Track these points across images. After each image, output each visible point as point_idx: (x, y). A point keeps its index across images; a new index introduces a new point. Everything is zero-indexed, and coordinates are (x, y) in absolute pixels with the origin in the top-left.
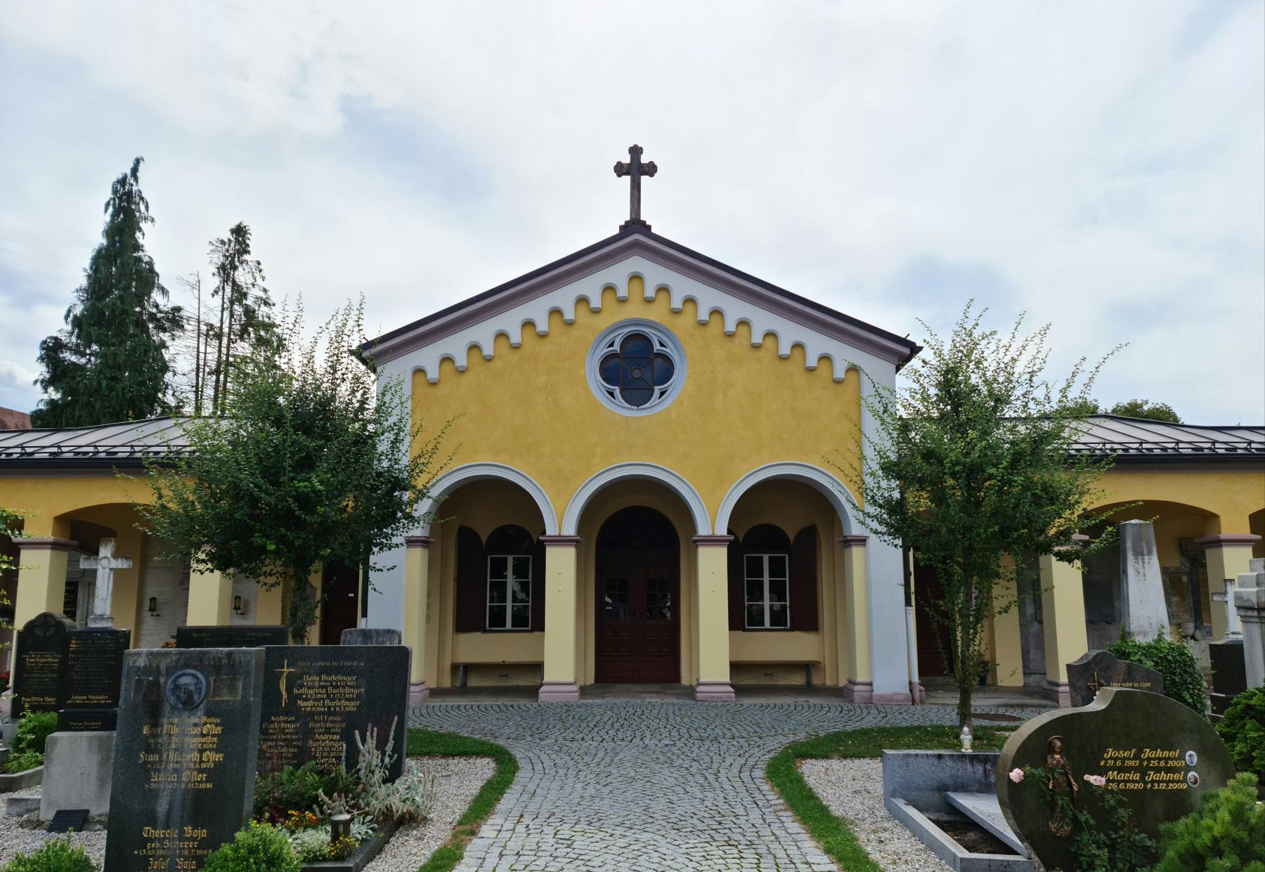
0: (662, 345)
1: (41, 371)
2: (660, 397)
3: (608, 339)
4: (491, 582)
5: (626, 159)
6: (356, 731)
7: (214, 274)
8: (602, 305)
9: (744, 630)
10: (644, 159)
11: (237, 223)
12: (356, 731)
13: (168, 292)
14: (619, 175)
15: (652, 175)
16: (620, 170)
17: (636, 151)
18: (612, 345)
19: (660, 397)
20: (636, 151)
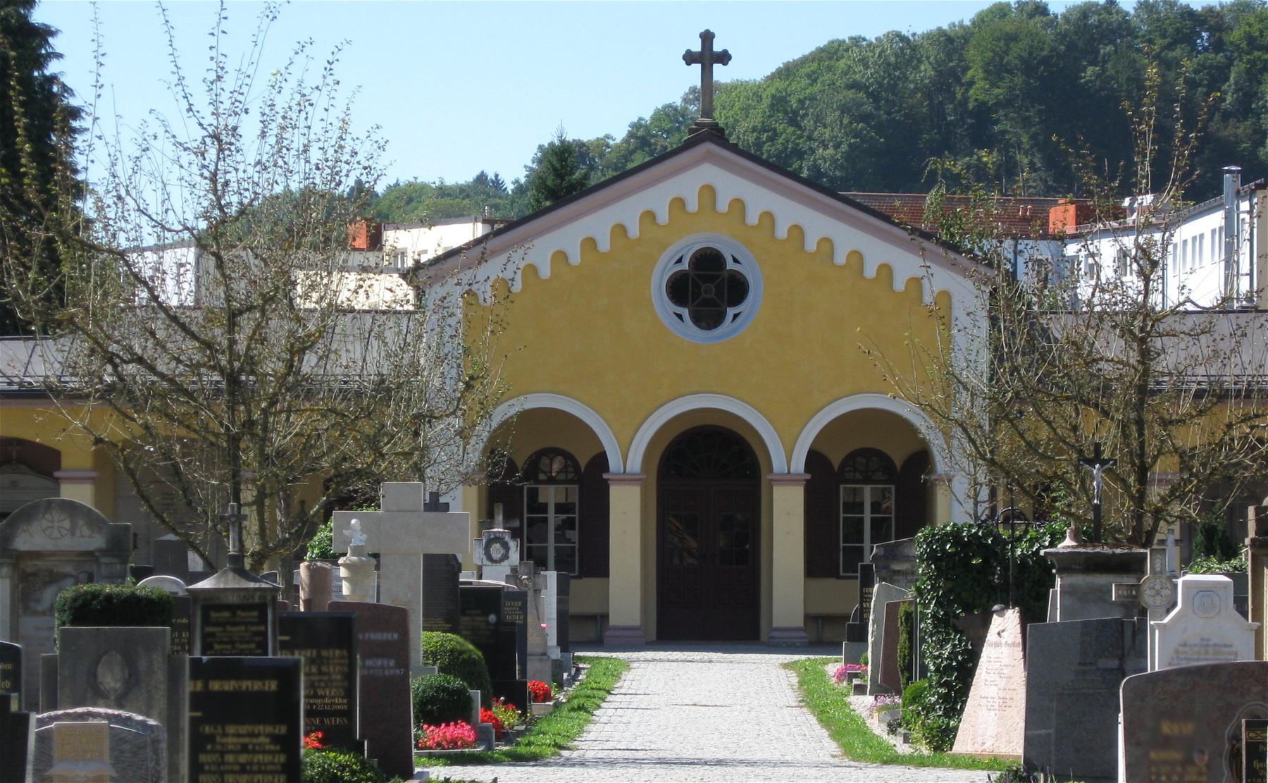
0: (735, 260)
1: (399, 246)
2: (682, 257)
3: (739, 320)
4: (528, 518)
5: (696, 47)
6: (396, 636)
7: (416, 178)
8: (972, 763)
9: (838, 577)
10: (717, 47)
11: (478, 172)
12: (396, 636)
13: (71, 90)
14: (688, 64)
15: (725, 64)
16: (690, 58)
17: (707, 37)
18: (736, 316)
19: (682, 257)
20: (707, 37)
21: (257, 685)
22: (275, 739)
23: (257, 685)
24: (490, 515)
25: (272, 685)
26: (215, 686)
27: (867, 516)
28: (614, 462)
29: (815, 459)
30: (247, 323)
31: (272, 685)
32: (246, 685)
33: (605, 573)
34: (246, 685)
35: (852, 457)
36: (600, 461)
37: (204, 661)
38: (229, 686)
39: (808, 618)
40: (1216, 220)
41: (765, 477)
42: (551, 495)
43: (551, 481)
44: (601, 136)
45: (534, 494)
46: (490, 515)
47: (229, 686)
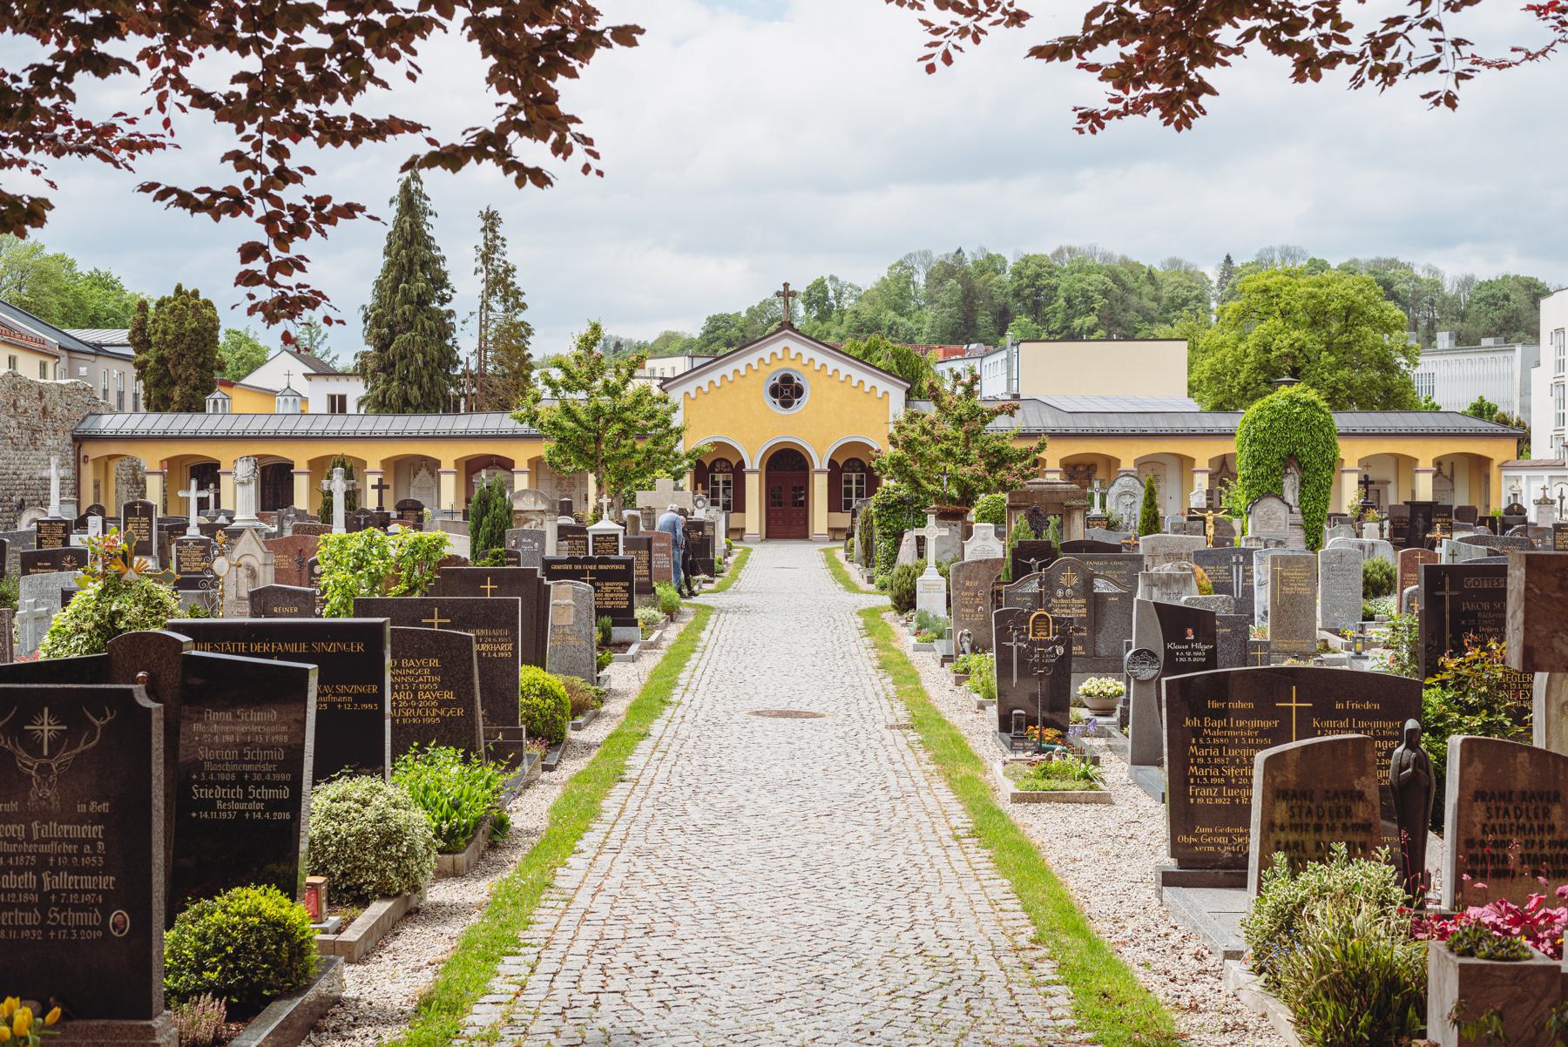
5: (782, 289)
17: (786, 285)
20: (786, 285)
21: (617, 567)
22: (624, 588)
23: (617, 567)
24: (696, 488)
25: (623, 567)
26: (601, 567)
27: (854, 486)
28: (748, 466)
29: (832, 463)
30: (959, 832)
31: (623, 567)
32: (612, 567)
33: (743, 511)
34: (612, 567)
35: (847, 462)
36: (741, 463)
37: (376, 11)
38: (606, 567)
39: (830, 529)
40: (1003, 355)
41: (811, 470)
42: (720, 478)
43: (721, 472)
44: (18, 194)
45: (713, 477)
46: (696, 488)
47: (606, 567)
